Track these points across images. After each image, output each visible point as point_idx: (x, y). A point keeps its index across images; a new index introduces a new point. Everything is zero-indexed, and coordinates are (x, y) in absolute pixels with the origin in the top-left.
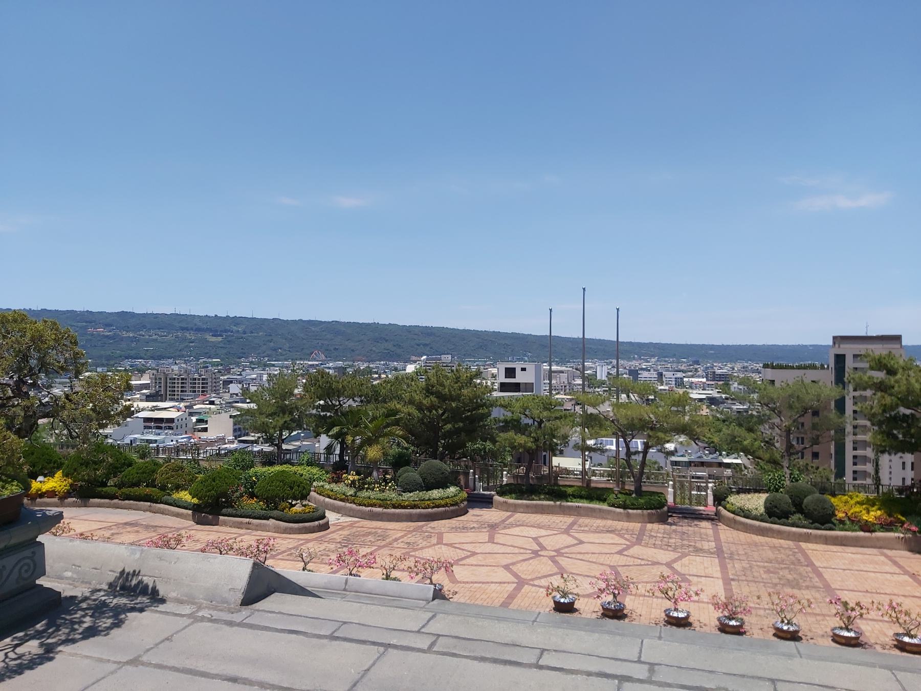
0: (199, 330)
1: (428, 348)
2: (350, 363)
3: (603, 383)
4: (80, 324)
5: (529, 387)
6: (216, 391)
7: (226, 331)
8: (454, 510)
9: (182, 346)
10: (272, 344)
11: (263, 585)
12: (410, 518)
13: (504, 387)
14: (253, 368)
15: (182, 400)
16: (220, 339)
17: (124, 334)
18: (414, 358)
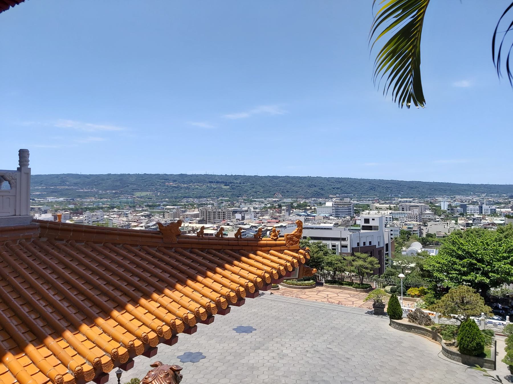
0: (218, 182)
1: (339, 190)
2: (295, 199)
3: (444, 212)
4: (162, 181)
5: (376, 228)
6: (229, 218)
7: (231, 183)
8: (311, 287)
9: (210, 191)
10: (254, 190)
11: (271, 293)
12: (299, 288)
13: (364, 228)
14: (245, 203)
15: (215, 223)
16: (228, 187)
17: (183, 185)
18: (331, 196)
